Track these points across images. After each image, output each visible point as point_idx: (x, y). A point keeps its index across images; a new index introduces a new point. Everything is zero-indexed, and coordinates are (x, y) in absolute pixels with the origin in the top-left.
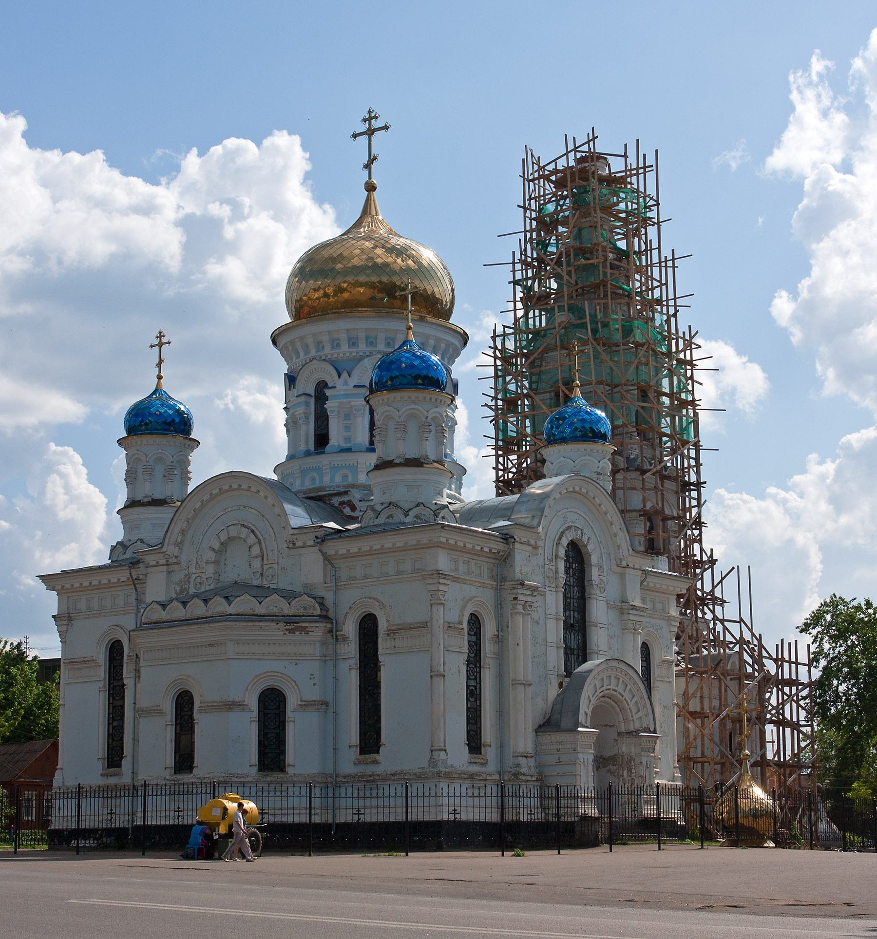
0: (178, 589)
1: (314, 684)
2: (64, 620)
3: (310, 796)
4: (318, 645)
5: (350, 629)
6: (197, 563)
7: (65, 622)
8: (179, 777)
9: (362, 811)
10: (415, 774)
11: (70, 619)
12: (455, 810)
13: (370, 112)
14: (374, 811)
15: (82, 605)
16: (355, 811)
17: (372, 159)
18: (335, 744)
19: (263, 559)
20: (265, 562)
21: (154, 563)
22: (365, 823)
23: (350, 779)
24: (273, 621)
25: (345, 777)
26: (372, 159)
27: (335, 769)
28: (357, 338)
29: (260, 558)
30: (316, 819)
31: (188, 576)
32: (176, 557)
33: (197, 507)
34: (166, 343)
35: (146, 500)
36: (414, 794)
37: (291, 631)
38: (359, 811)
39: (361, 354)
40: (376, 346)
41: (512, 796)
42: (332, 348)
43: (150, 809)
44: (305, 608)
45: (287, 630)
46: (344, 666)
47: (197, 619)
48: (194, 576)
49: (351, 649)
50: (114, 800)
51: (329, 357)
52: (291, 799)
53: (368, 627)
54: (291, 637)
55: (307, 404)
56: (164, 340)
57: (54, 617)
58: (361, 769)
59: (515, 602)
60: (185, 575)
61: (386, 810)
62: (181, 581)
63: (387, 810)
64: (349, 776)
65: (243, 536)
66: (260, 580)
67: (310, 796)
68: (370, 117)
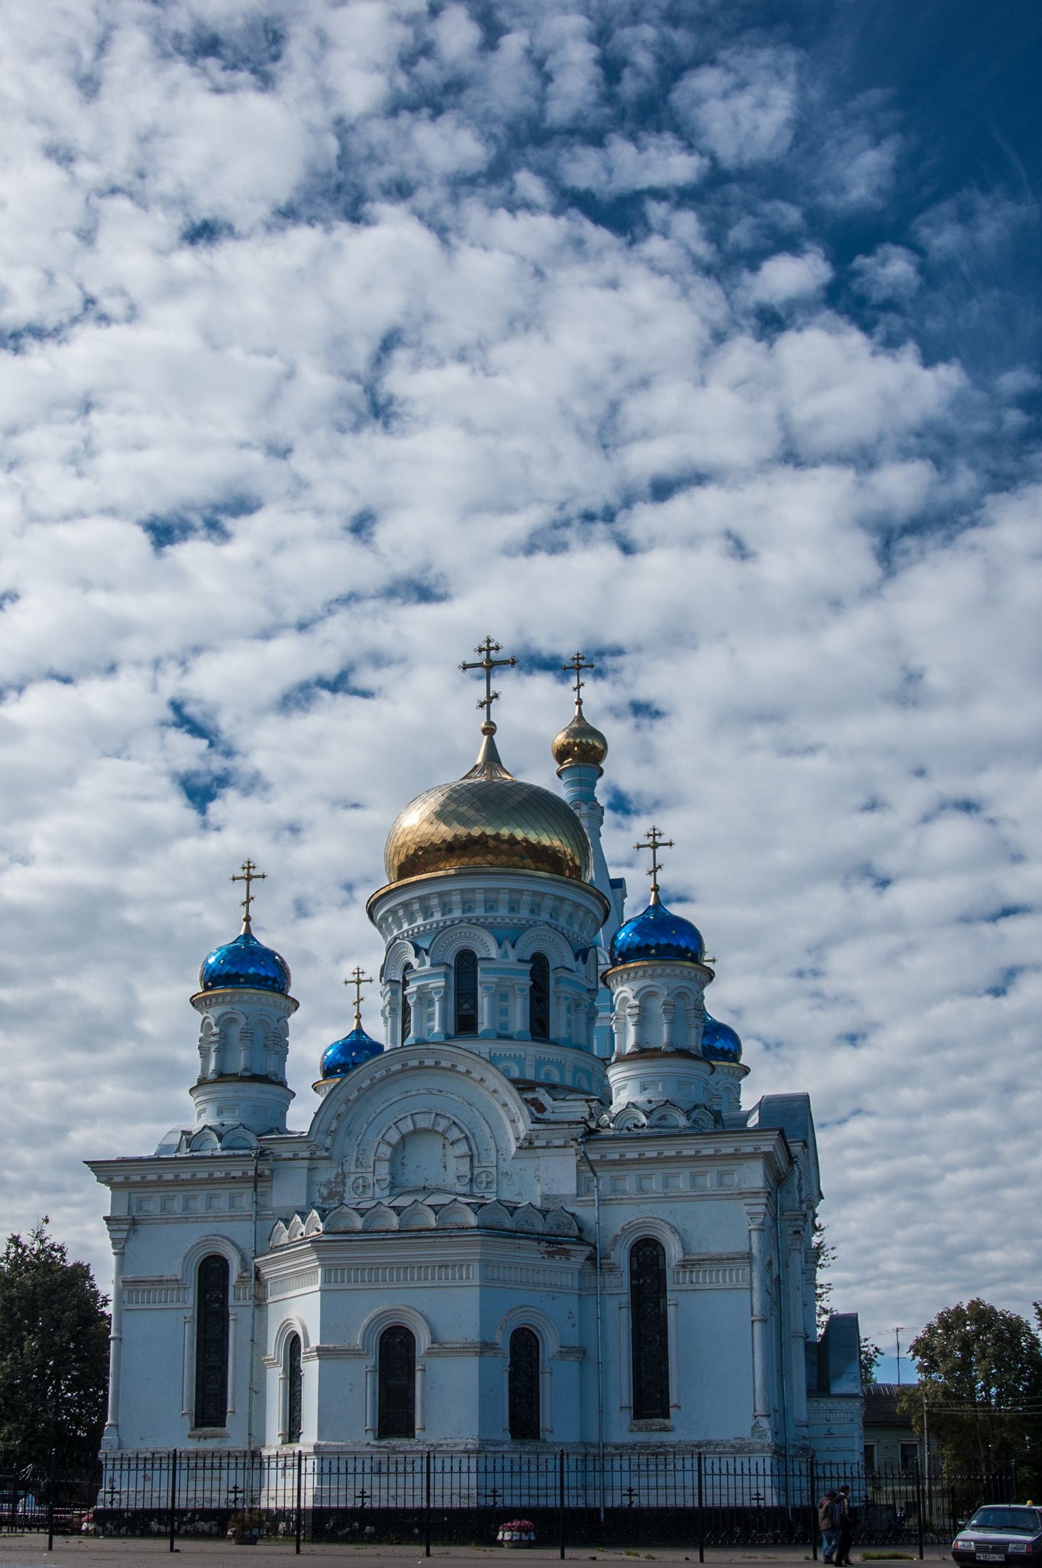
0: (325, 1191)
1: (573, 1326)
2: (124, 1227)
3: (700, 1470)
4: (576, 1275)
5: (621, 1257)
6: (357, 1159)
7: (127, 1227)
8: (384, 1443)
9: (500, 1492)
10: (733, 1446)
11: (134, 1222)
12: (758, 1494)
13: (489, 641)
14: (661, 1492)
15: (153, 1206)
16: (489, 1492)
17: (249, 899)
18: (600, 1405)
19: (472, 1160)
20: (476, 1164)
21: (290, 1155)
22: (640, 1510)
23: (623, 1449)
24: (535, 1239)
25: (617, 1447)
26: (249, 899)
27: (601, 1438)
28: (496, 902)
29: (468, 1159)
30: (571, 1502)
31: (344, 1176)
32: (327, 1149)
33: (364, 1085)
34: (258, 877)
35: (247, 1074)
36: (439, 1469)
37: (551, 1254)
38: (494, 1491)
39: (523, 922)
40: (539, 915)
41: (452, 1472)
42: (443, 915)
43: (183, 1488)
44: (559, 1226)
45: (546, 1252)
46: (612, 1304)
47: (420, 1230)
48: (352, 1178)
49: (620, 1284)
50: (401, 1479)
51: (482, 920)
52: (679, 1474)
53: (647, 1256)
54: (548, 1262)
55: (446, 976)
56: (253, 872)
57: (107, 1219)
58: (641, 1437)
59: (797, 1236)
60: (338, 1175)
61: (671, 1490)
62: (329, 1182)
63: (671, 1491)
64: (623, 1446)
65: (440, 1129)
66: (468, 1187)
67: (700, 1470)
68: (249, 866)
